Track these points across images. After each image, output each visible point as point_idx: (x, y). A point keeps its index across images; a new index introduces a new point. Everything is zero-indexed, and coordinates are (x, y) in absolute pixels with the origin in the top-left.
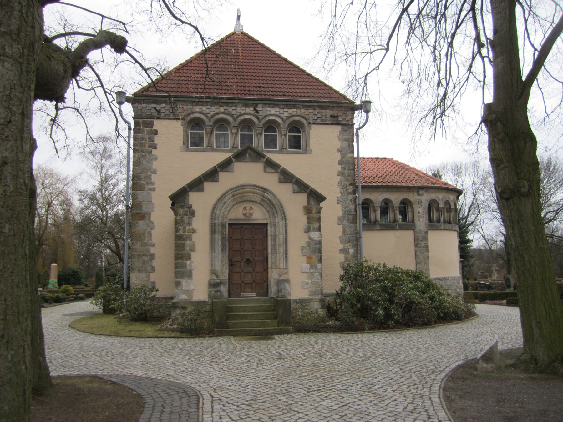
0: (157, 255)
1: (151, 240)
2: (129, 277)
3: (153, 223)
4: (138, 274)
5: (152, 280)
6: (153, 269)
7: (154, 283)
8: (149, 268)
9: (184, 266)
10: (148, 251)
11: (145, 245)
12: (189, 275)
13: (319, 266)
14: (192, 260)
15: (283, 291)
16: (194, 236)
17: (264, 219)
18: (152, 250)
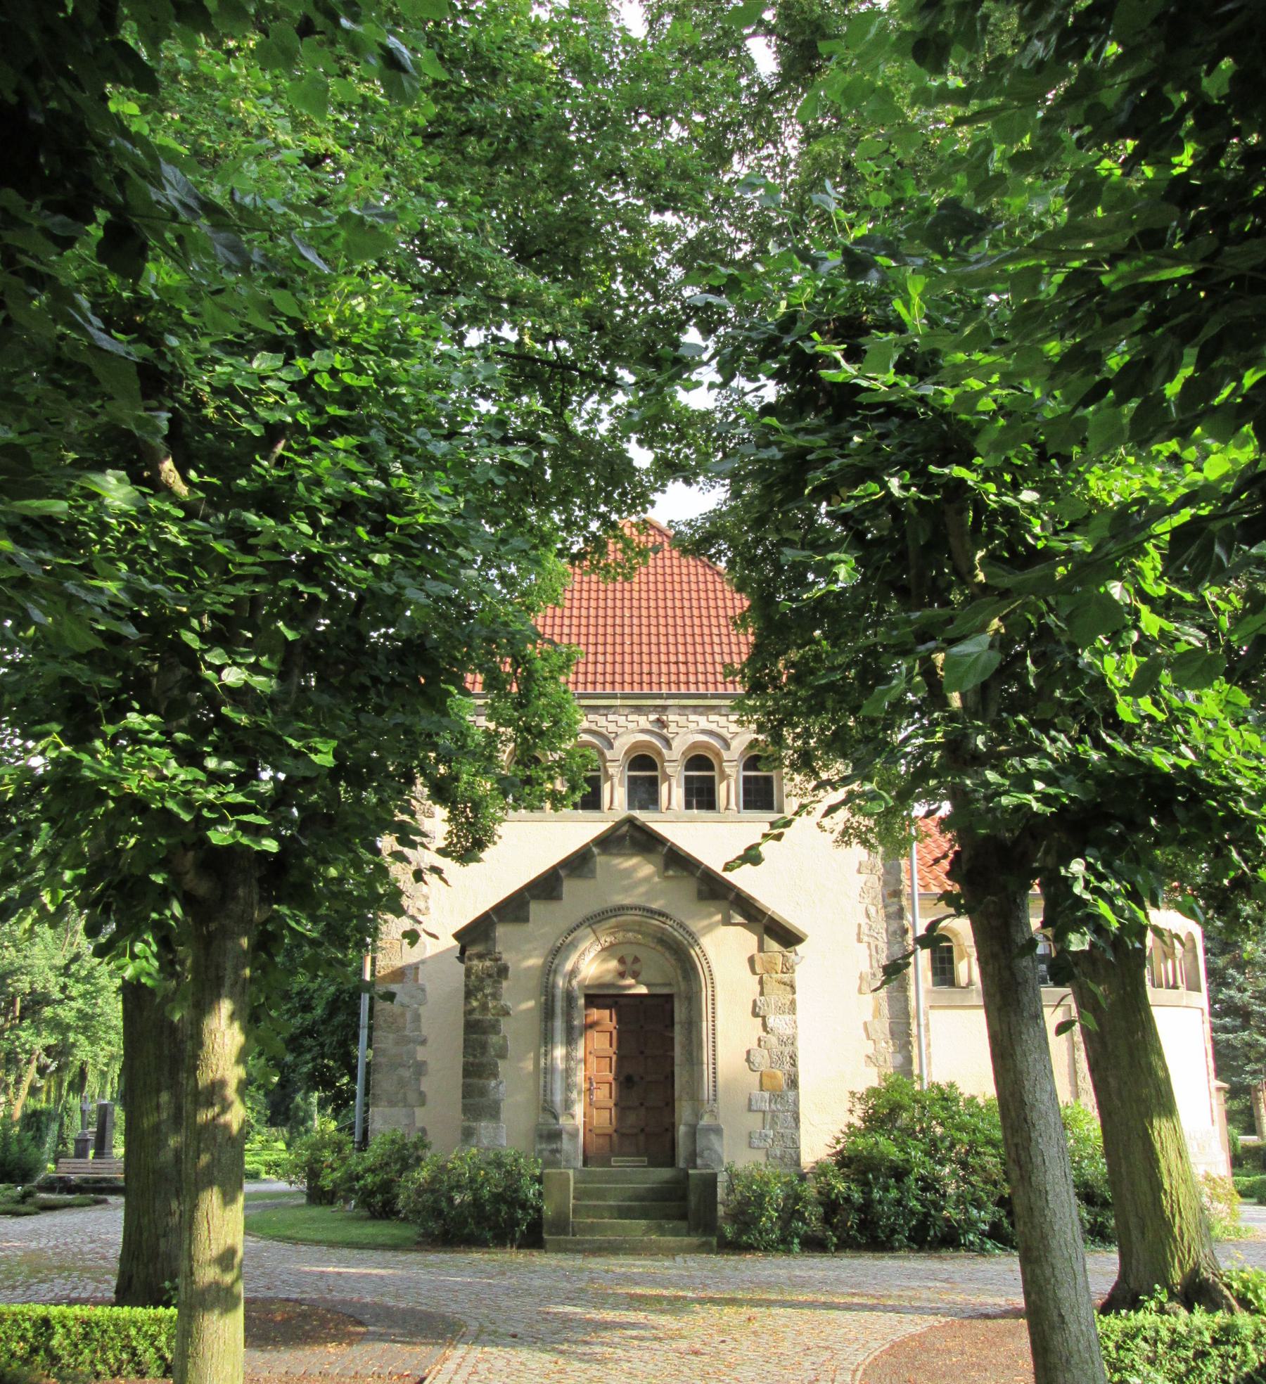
0: (432, 1065)
1: (418, 1029)
2: (365, 1120)
3: (423, 990)
4: (387, 1110)
5: (419, 1124)
6: (422, 1099)
7: (423, 1130)
8: (412, 1097)
9: (483, 1092)
10: (412, 1055)
11: (403, 1041)
12: (493, 1112)
13: (791, 1094)
14: (501, 1077)
15: (706, 1153)
16: (504, 1024)
17: (665, 985)
18: (421, 1054)
